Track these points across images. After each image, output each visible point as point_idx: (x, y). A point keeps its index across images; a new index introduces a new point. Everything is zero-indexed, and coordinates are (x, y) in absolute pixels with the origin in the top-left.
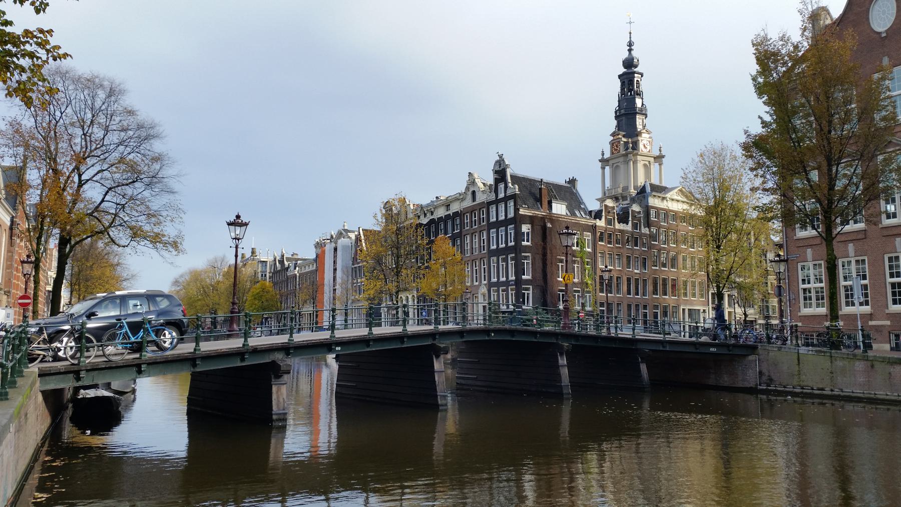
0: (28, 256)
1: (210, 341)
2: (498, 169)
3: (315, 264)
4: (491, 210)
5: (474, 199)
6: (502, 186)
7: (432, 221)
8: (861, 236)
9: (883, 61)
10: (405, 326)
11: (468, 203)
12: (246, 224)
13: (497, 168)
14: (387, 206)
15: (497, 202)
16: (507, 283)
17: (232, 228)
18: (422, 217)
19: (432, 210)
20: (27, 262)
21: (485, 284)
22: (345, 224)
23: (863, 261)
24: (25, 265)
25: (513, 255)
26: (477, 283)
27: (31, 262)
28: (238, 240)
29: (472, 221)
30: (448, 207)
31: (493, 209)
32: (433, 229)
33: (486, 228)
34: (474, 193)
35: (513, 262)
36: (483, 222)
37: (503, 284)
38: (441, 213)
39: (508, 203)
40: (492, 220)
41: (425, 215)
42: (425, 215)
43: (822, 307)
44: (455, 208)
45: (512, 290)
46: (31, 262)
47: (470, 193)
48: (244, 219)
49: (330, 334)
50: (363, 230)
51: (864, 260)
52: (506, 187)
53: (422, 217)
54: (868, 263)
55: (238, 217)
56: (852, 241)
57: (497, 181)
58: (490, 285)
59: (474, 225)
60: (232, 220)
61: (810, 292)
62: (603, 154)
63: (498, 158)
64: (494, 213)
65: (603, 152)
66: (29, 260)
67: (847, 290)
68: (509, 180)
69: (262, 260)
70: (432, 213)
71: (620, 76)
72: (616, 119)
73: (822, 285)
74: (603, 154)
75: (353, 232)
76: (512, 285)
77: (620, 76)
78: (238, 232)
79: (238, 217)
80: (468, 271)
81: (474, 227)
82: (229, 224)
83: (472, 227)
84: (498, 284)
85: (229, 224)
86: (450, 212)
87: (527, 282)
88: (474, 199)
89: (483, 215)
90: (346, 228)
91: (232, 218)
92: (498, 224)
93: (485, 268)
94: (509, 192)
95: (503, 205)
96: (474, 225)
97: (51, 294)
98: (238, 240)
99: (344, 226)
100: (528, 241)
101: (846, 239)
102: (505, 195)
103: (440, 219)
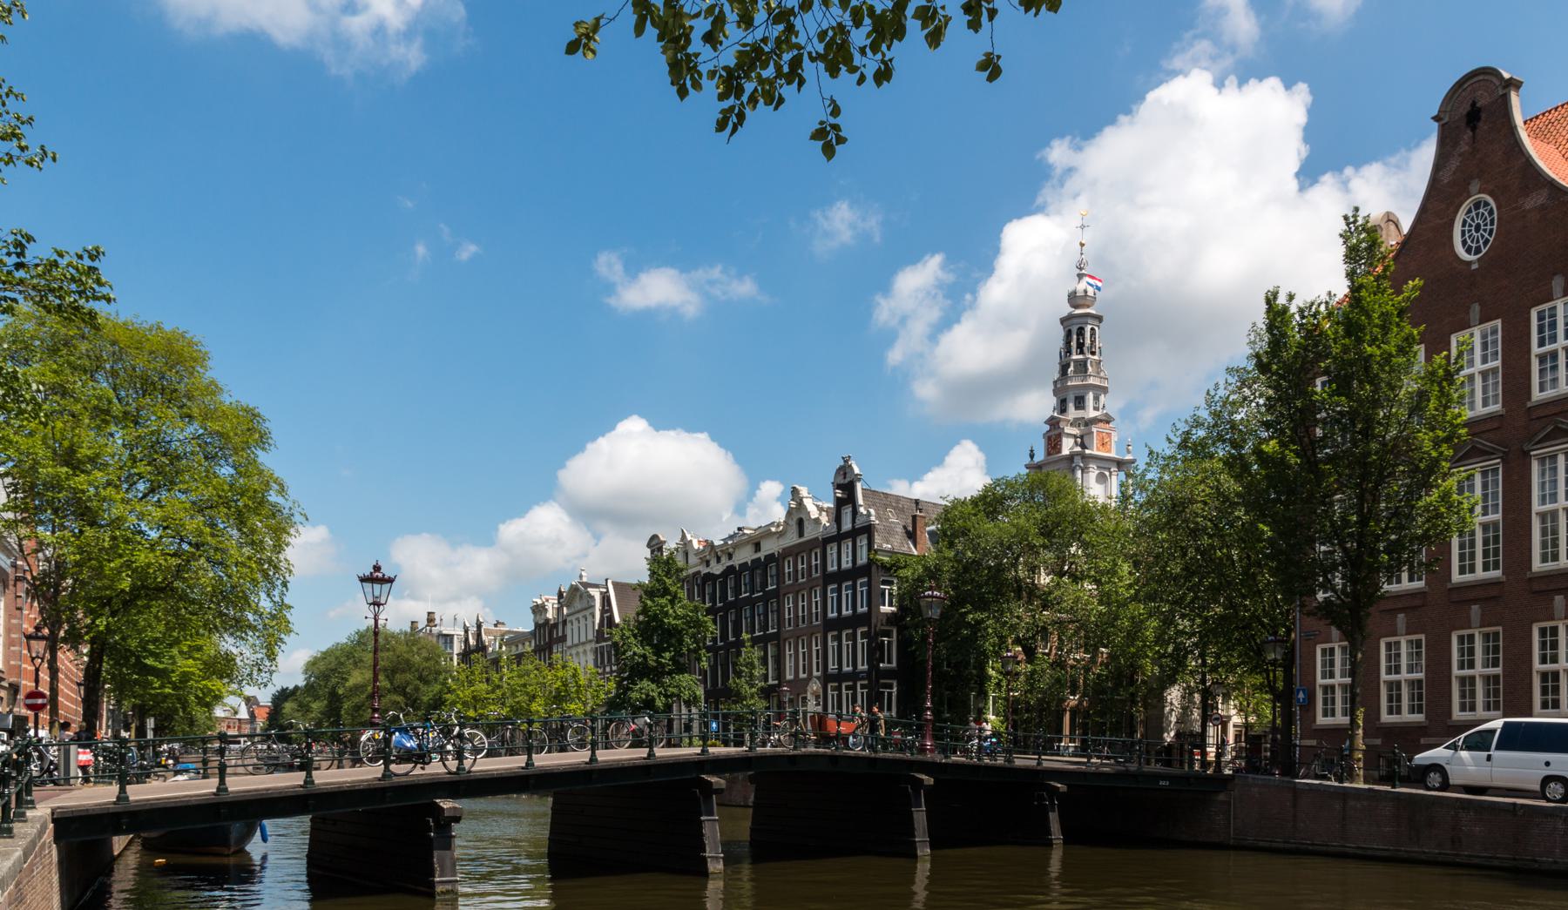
0: (38, 628)
1: (500, 755)
2: (842, 482)
3: (533, 642)
4: (829, 551)
5: (801, 534)
6: (847, 512)
7: (730, 570)
8: (1417, 602)
9: (1471, 311)
10: (651, 748)
11: (792, 539)
12: (390, 581)
13: (841, 480)
14: (654, 543)
15: (839, 538)
16: (854, 676)
17: (368, 586)
18: (713, 562)
19: (731, 550)
20: (36, 638)
21: (818, 678)
22: (583, 573)
23: (1496, 634)
24: (33, 642)
25: (866, 629)
26: (805, 676)
27: (43, 638)
28: (379, 606)
29: (797, 571)
30: (757, 547)
31: (832, 551)
32: (730, 583)
33: (821, 582)
34: (800, 523)
35: (865, 640)
36: (816, 572)
37: (847, 677)
38: (745, 556)
39: (858, 541)
40: (830, 569)
41: (719, 559)
42: (719, 559)
43: (1418, 713)
44: (769, 547)
45: (863, 687)
46: (43, 638)
47: (793, 523)
48: (387, 571)
49: (217, 784)
50: (613, 583)
51: (1498, 633)
52: (855, 512)
53: (713, 562)
54: (1426, 646)
55: (377, 568)
56: (1475, 601)
57: (840, 503)
58: (826, 678)
59: (800, 576)
60: (367, 573)
61: (1333, 692)
62: (1032, 456)
63: (842, 463)
64: (835, 556)
65: (1032, 451)
66: (40, 634)
67: (1325, 692)
68: (860, 501)
69: (444, 632)
70: (730, 556)
71: (1063, 321)
72: (1055, 395)
73: (1498, 670)
74: (1032, 456)
75: (596, 586)
76: (863, 679)
77: (1063, 321)
78: (377, 593)
79: (377, 568)
80: (790, 655)
81: (800, 581)
82: (363, 580)
83: (797, 580)
84: (840, 677)
85: (363, 580)
86: (762, 555)
87: (889, 674)
88: (801, 534)
89: (816, 560)
90: (585, 580)
91: (368, 571)
92: (840, 576)
93: (818, 651)
94: (859, 523)
95: (850, 544)
96: (800, 576)
97: (82, 688)
98: (379, 606)
99: (581, 576)
100: (891, 605)
101: (1551, 587)
102: (853, 526)
103: (744, 566)
